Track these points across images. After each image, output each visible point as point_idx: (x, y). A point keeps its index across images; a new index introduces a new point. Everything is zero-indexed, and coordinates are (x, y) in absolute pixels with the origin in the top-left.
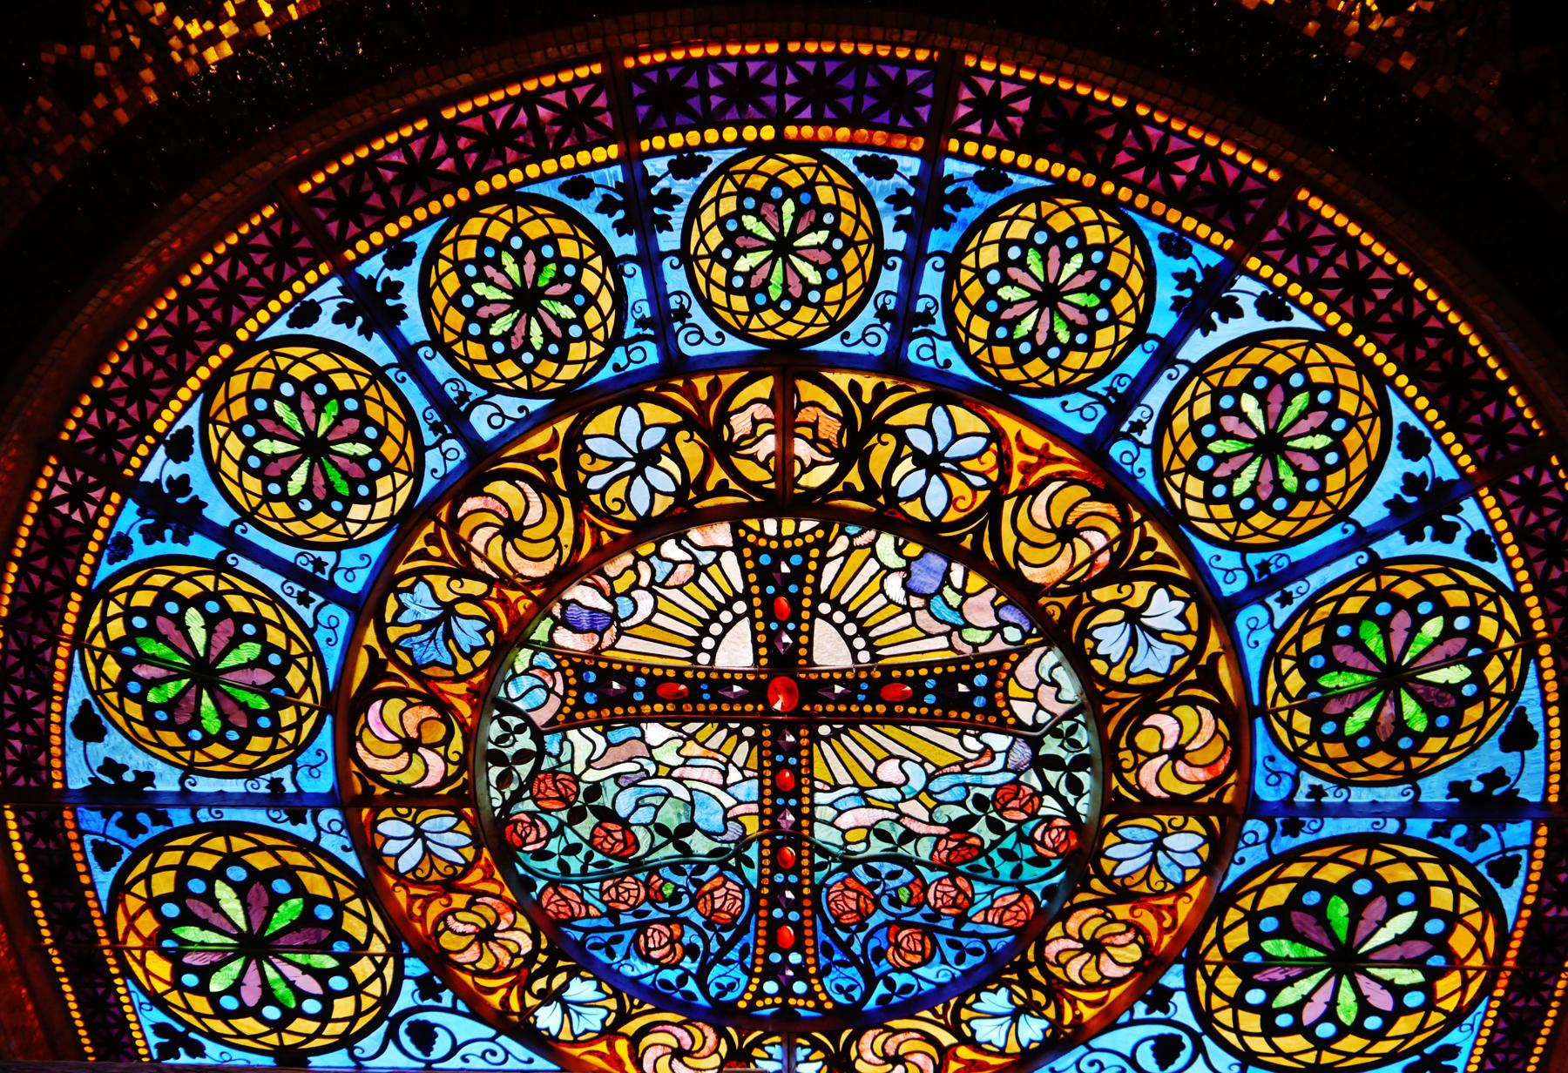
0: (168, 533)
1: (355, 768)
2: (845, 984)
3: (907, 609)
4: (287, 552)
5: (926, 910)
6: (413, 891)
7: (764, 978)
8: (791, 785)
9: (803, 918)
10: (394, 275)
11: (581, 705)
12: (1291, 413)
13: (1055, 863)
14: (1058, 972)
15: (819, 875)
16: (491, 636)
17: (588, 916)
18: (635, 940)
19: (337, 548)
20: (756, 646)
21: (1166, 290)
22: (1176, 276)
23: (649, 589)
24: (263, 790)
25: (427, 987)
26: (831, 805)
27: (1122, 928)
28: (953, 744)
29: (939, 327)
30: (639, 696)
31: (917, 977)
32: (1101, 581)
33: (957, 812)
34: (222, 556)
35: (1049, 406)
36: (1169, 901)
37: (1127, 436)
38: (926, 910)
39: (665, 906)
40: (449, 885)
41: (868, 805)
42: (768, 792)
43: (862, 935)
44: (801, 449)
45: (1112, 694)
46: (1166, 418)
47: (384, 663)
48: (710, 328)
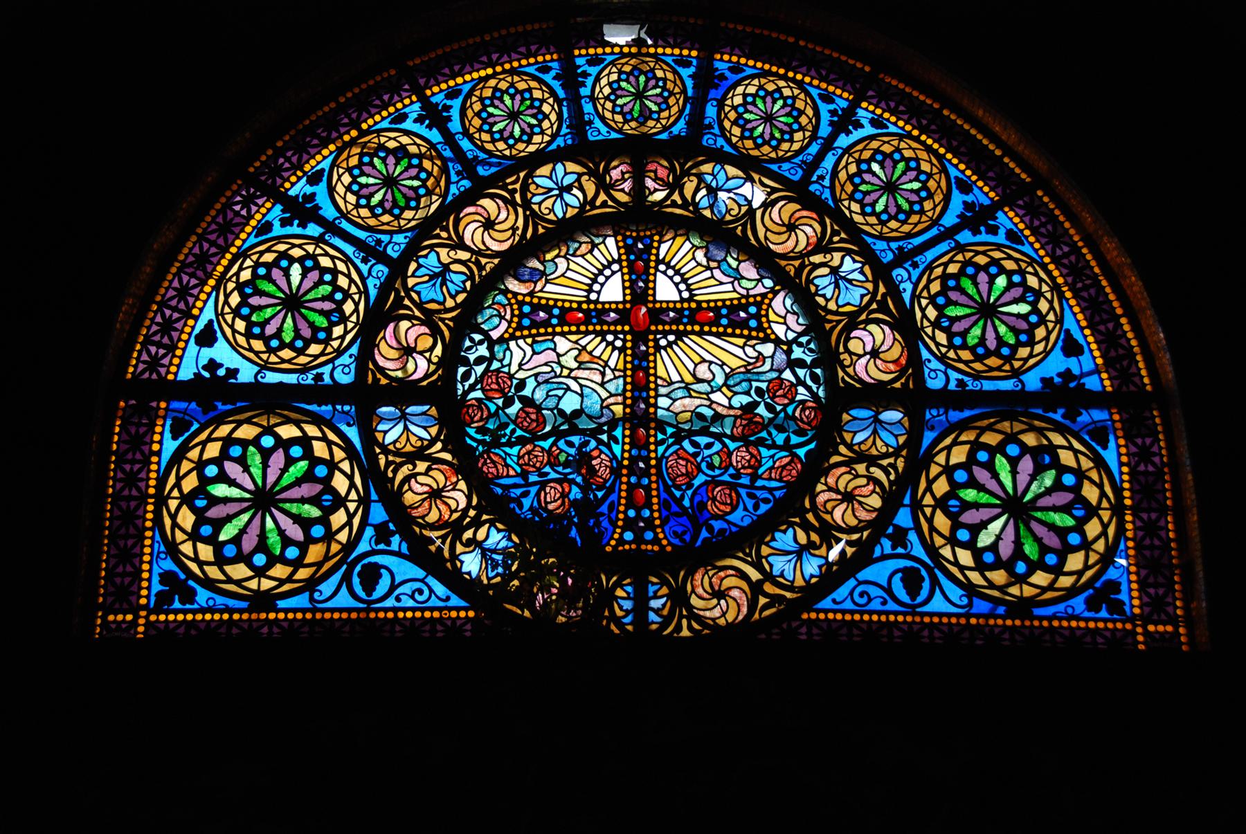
0: (296, 222)
1: (371, 366)
2: (679, 529)
3: (708, 268)
4: (362, 235)
5: (732, 471)
6: (391, 458)
7: (624, 529)
8: (644, 382)
9: (650, 482)
10: (449, 103)
11: (520, 327)
12: (898, 173)
13: (810, 434)
14: (828, 517)
15: (661, 449)
16: (468, 284)
17: (508, 476)
18: (538, 494)
19: (391, 233)
20: (624, 288)
21: (825, 117)
22: (829, 111)
23: (564, 257)
24: (310, 381)
25: (382, 534)
26: (667, 396)
27: (864, 481)
28: (739, 352)
29: (716, 131)
30: (554, 321)
31: (728, 522)
32: (814, 252)
33: (745, 400)
34: (322, 235)
35: (774, 167)
36: (891, 460)
37: (816, 182)
38: (732, 471)
39: (560, 469)
40: (412, 458)
41: (691, 396)
42: (629, 387)
43: (689, 492)
44: (650, 183)
45: (829, 317)
46: (835, 173)
47: (403, 298)
48: (604, 129)
